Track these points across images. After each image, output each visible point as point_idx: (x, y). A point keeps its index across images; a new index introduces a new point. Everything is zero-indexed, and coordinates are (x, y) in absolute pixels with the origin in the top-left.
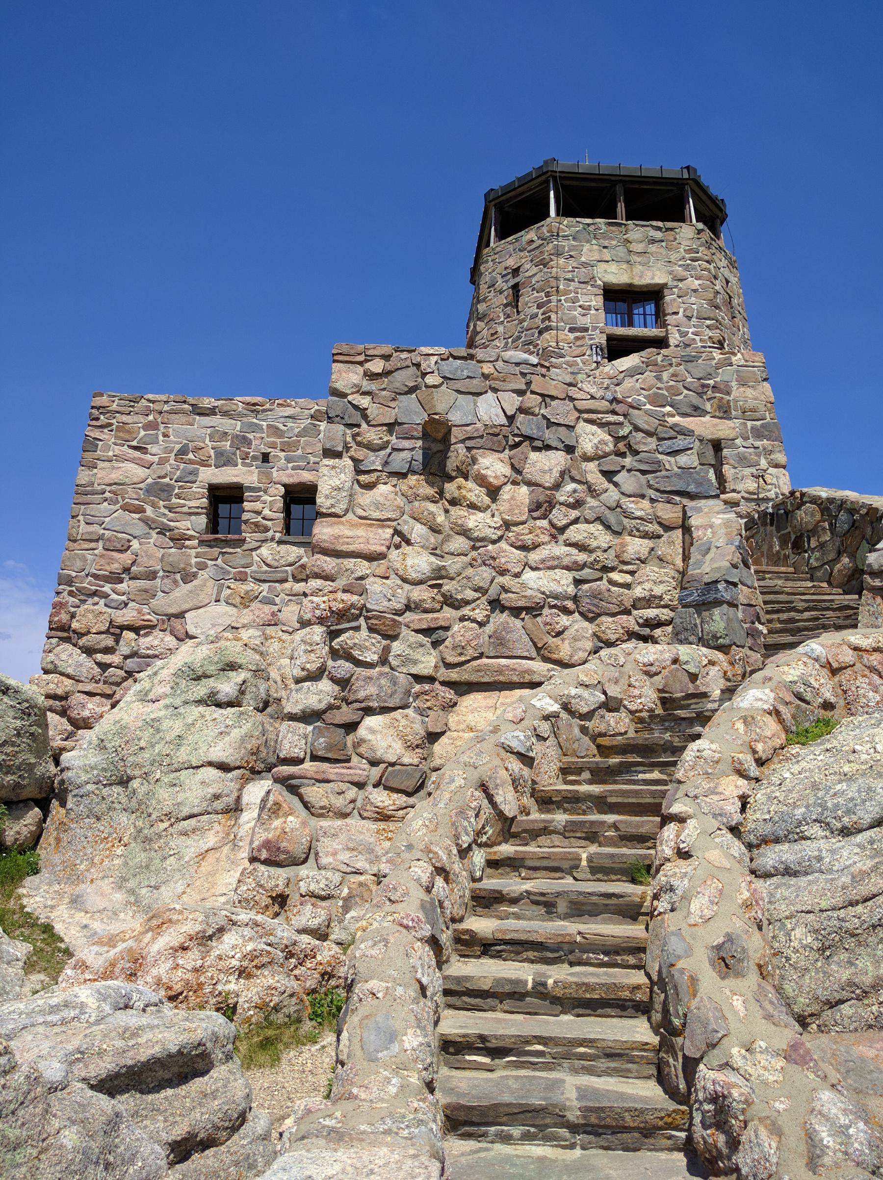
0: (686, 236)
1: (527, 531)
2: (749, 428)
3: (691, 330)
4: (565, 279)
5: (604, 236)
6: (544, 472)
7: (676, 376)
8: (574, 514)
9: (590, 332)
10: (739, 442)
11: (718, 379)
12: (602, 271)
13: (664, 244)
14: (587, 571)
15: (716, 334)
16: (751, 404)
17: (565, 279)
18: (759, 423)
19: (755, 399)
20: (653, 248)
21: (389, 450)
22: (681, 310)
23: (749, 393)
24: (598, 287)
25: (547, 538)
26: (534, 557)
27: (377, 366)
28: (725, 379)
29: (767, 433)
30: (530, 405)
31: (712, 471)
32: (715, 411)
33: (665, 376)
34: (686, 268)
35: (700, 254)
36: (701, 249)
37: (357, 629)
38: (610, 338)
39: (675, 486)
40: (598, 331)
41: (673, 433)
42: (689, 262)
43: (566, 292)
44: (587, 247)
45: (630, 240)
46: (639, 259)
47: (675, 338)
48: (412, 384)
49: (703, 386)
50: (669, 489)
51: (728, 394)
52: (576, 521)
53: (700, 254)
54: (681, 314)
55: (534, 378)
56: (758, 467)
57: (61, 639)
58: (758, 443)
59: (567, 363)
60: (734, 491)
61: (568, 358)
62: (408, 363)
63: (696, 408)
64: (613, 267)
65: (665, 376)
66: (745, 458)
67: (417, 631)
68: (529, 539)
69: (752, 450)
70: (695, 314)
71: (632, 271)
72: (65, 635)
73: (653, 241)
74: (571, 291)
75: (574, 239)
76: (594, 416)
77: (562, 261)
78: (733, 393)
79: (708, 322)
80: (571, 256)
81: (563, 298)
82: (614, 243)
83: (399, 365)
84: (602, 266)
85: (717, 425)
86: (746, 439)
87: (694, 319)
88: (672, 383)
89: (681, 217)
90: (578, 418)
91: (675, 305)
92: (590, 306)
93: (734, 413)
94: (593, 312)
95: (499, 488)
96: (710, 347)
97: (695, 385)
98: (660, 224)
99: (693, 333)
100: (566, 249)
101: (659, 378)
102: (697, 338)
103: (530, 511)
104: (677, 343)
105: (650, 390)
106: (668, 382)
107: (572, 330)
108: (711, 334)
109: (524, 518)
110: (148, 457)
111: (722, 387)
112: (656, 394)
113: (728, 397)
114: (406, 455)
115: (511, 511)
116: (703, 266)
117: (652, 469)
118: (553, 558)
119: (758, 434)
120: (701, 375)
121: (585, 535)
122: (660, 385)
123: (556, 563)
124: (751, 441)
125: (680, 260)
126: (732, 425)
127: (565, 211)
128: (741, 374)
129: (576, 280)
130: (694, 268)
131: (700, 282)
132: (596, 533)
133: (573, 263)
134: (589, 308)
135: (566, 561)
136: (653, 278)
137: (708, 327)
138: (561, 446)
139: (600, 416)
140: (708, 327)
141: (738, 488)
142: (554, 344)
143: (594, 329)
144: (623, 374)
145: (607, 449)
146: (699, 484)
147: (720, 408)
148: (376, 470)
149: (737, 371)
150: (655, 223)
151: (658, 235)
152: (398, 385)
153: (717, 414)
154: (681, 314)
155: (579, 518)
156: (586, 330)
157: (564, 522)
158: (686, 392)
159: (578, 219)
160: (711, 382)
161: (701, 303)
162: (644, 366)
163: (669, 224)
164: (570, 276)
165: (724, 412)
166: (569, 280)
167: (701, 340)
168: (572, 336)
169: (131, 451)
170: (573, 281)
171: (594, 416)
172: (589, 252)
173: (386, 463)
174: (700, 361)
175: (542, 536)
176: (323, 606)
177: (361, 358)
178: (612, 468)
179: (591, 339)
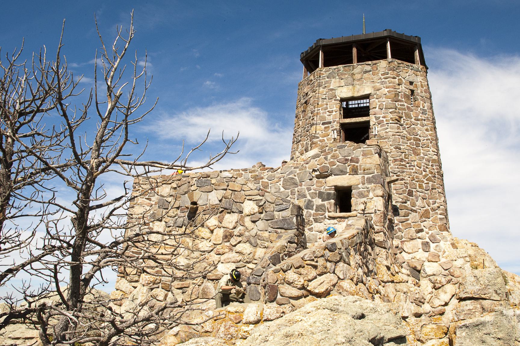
0: (382, 66)
1: (221, 248)
2: (366, 178)
3: (381, 116)
4: (322, 99)
5: (342, 74)
6: (229, 222)
7: (334, 156)
8: (240, 239)
9: (332, 124)
10: (360, 186)
11: (353, 156)
12: (340, 92)
13: (371, 73)
14: (241, 263)
15: (395, 116)
16: (368, 166)
17: (322, 99)
18: (371, 176)
19: (370, 164)
20: (366, 75)
21: (177, 217)
22: (378, 106)
23: (368, 160)
24: (337, 100)
25: (227, 250)
26: (223, 258)
27: (174, 185)
28: (357, 155)
29: (374, 180)
30: (227, 195)
31: (295, 218)
32: (351, 172)
33: (329, 156)
34: (382, 83)
35: (389, 75)
36: (390, 72)
37: (158, 287)
38: (368, 115)
39: (279, 225)
40: (336, 123)
41: (281, 202)
42: (383, 80)
43: (322, 105)
44: (333, 80)
45: (354, 73)
46: (358, 83)
47: (373, 121)
48: (187, 190)
49: (347, 160)
50: (276, 227)
51: (357, 163)
52: (240, 242)
53: (389, 75)
54: (377, 108)
55: (230, 183)
56: (367, 198)
57: (122, 277)
58: (369, 186)
59: (320, 141)
60: (355, 210)
61: (321, 138)
62: (186, 182)
63: (342, 171)
64: (345, 89)
65: (329, 156)
66: (362, 194)
67: (177, 289)
68: (221, 251)
69: (366, 189)
70: (384, 107)
71: (354, 89)
72: (123, 275)
73: (366, 72)
74: (324, 104)
75: (328, 78)
76: (250, 197)
77: (321, 89)
78: (360, 162)
79: (391, 110)
80: (326, 87)
81: (320, 108)
82: (346, 76)
83: (183, 183)
84: (340, 89)
85: (350, 178)
86: (363, 184)
87: (384, 110)
88: (332, 160)
89: (384, 56)
90: (246, 198)
91: (374, 103)
92: (333, 111)
93: (359, 171)
94: (334, 113)
95: (213, 230)
96: (391, 123)
97: (342, 160)
98: (370, 62)
99: (382, 117)
100: (324, 83)
101: (326, 159)
102: (384, 119)
103: (223, 239)
104: (374, 123)
105: (321, 164)
106: (330, 160)
107: (323, 124)
108: (392, 116)
109: (220, 242)
110: (151, 202)
111: (355, 159)
112: (324, 166)
113: (356, 164)
114: (182, 219)
115: (215, 240)
116: (390, 81)
117: (271, 219)
118: (228, 259)
119: (370, 181)
120: (346, 155)
121: (242, 248)
122: (326, 162)
123: (229, 260)
124: (366, 185)
125: (379, 80)
126: (358, 178)
127: (327, 64)
128: (365, 152)
129: (327, 98)
130: (385, 83)
131: (388, 90)
132: (246, 247)
133: (325, 90)
134: (332, 112)
135: (233, 260)
136: (364, 92)
137: (390, 113)
138: (237, 211)
139: (253, 197)
140: (390, 113)
141: (357, 209)
142: (314, 132)
143: (334, 121)
144: (310, 158)
145: (255, 211)
146: (289, 224)
147: (353, 170)
148: (171, 226)
149: (363, 151)
150: (367, 63)
151: (368, 68)
152: (181, 191)
153: (351, 173)
154: (377, 108)
155: (241, 241)
156: (330, 123)
157: (235, 243)
158: (338, 163)
159: (330, 67)
160: (350, 158)
161: (387, 101)
162: (320, 153)
163: (374, 62)
164: (324, 97)
165: (355, 171)
166: (324, 99)
167: (386, 120)
168: (323, 127)
169: (146, 200)
170: (326, 99)
171: (250, 197)
172: (334, 83)
173: (175, 223)
174: (346, 148)
175: (226, 249)
176: (148, 279)
177: (170, 182)
178: (255, 220)
179: (332, 127)
